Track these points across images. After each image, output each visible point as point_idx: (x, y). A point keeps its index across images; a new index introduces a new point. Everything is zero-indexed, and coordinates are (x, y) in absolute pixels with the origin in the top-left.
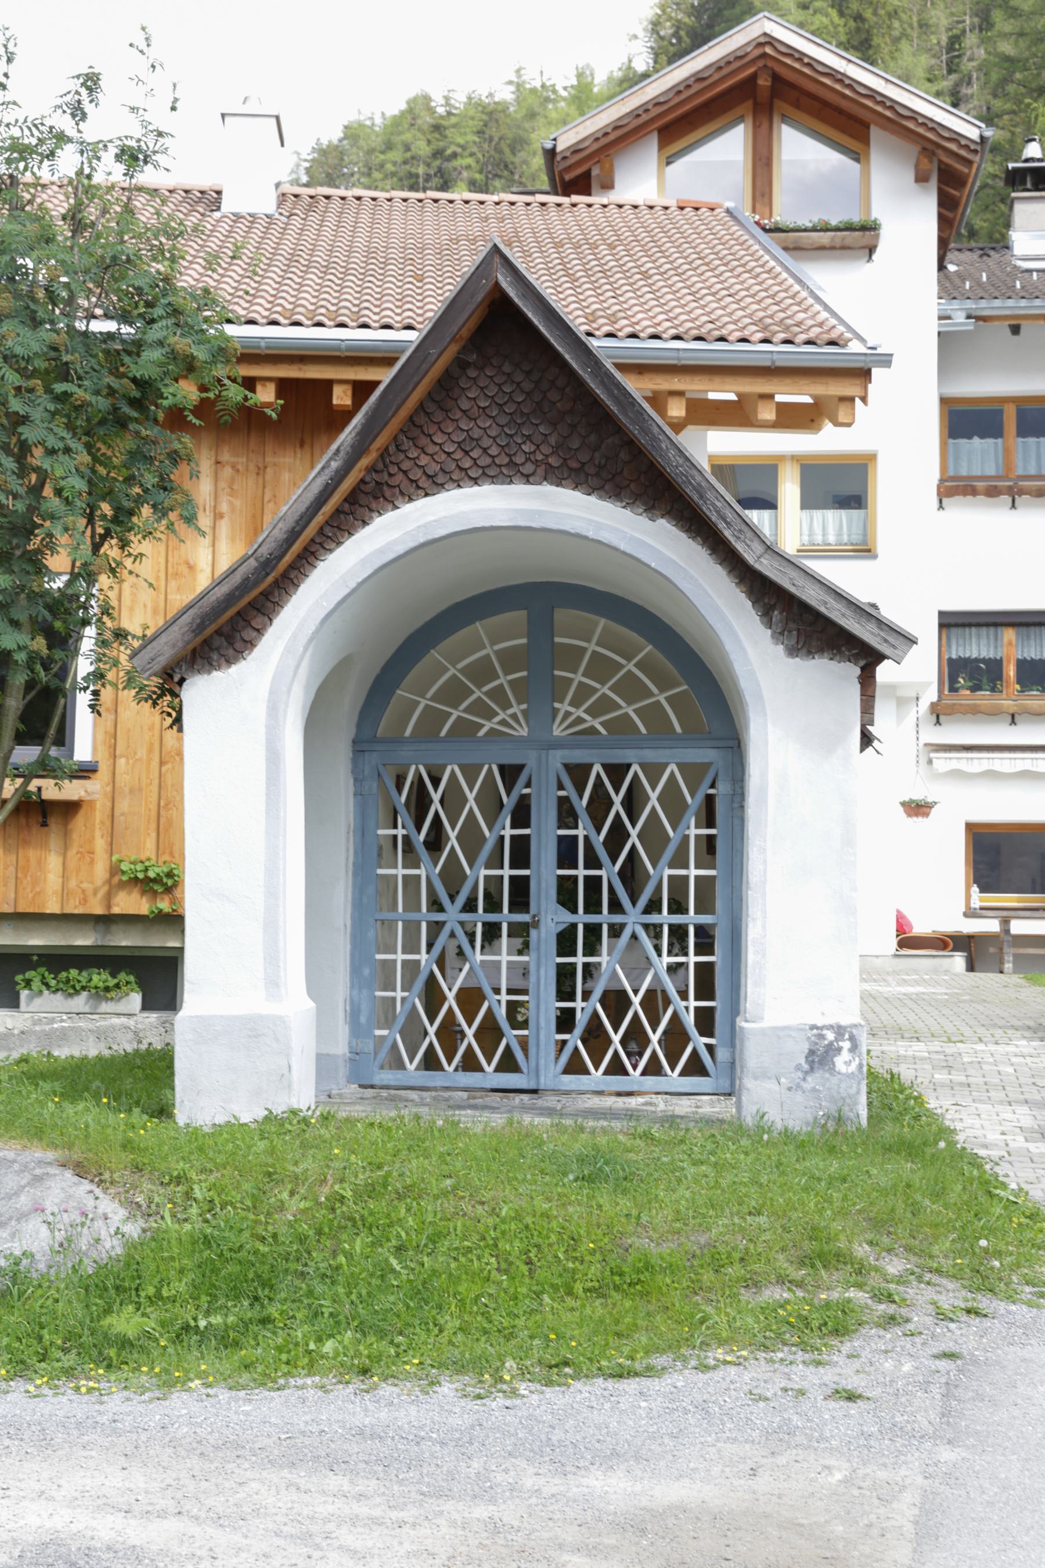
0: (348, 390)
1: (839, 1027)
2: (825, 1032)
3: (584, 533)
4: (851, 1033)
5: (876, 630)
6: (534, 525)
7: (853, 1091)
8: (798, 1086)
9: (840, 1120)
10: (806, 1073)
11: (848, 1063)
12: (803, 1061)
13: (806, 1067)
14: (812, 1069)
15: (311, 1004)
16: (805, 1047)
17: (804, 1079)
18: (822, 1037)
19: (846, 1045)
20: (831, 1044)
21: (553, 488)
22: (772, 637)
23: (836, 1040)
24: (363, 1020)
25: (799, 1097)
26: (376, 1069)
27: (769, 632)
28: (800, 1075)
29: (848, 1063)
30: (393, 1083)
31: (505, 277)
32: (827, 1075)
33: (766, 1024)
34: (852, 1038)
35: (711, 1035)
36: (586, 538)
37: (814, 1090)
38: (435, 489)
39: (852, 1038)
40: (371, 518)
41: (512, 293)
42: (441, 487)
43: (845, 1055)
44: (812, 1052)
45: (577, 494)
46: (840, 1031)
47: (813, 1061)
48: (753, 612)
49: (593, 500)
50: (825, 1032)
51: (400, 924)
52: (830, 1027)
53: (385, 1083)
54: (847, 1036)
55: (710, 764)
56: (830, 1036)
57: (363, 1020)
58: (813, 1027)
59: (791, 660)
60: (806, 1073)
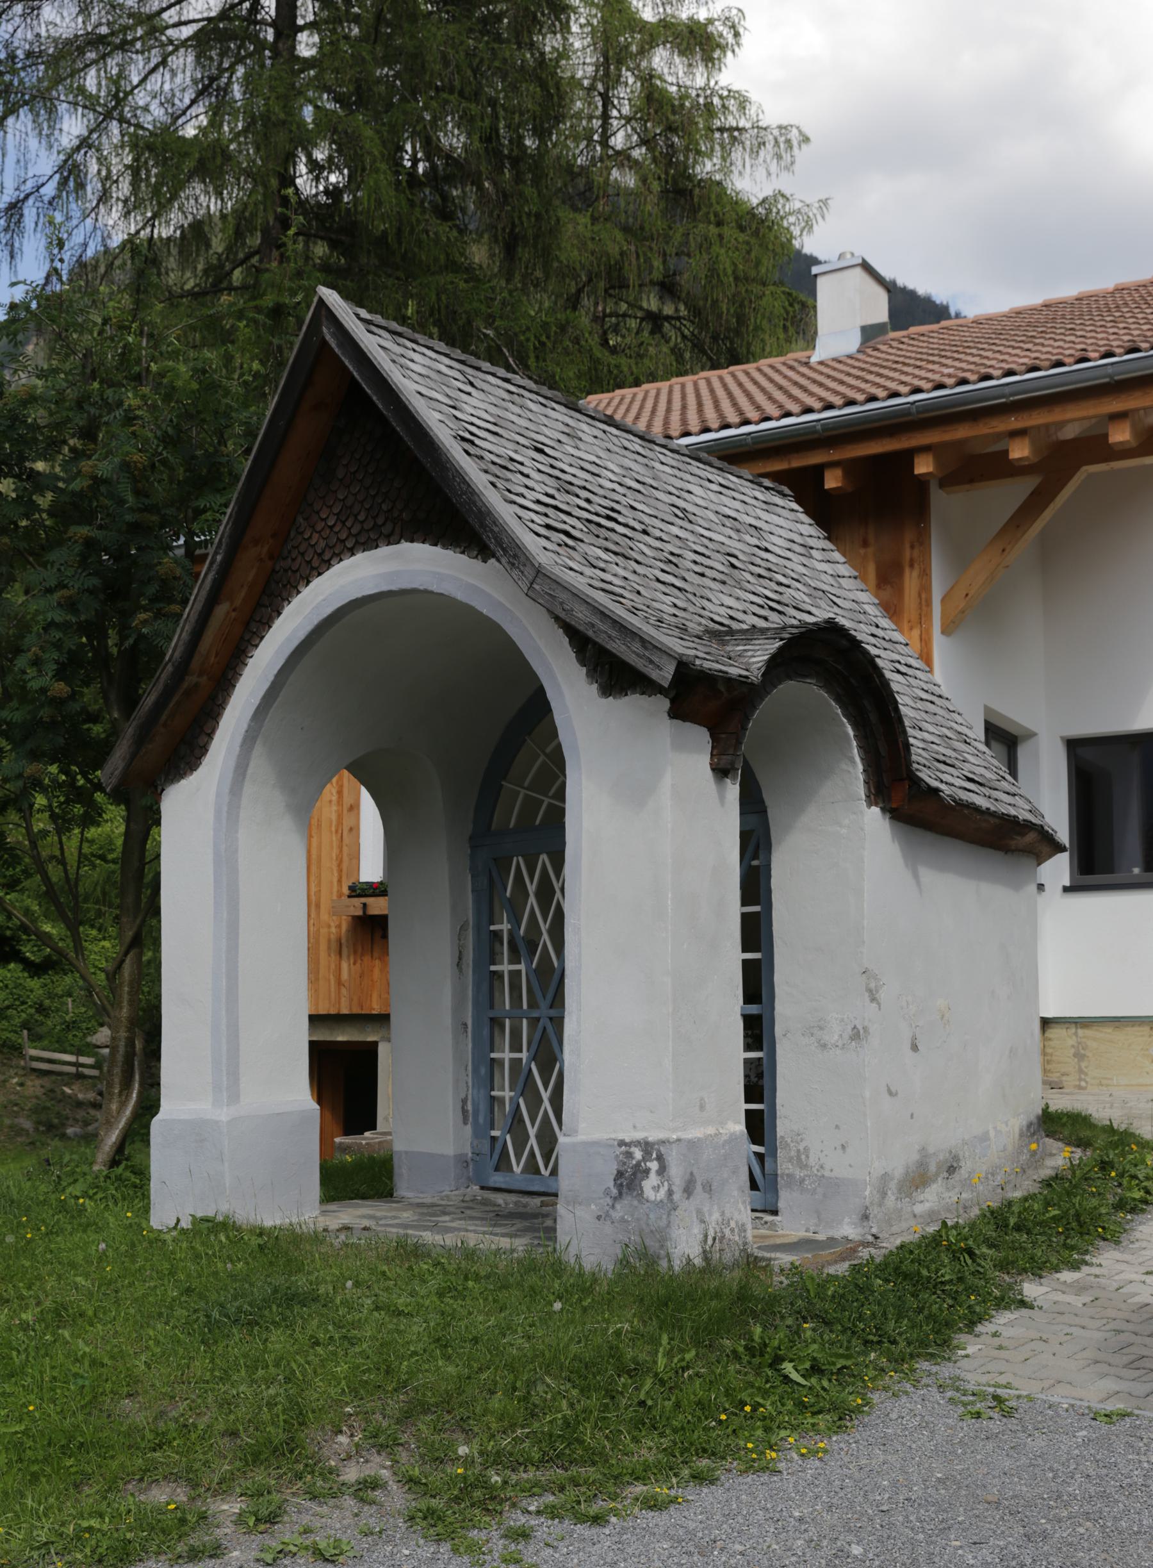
0: (838, 472)
1: (647, 1143)
2: (633, 1149)
3: (430, 588)
4: (659, 1151)
5: (641, 651)
6: (394, 588)
7: (663, 1223)
8: (607, 1215)
9: (650, 1260)
10: (615, 1199)
11: (656, 1189)
12: (611, 1184)
13: (615, 1191)
14: (620, 1194)
15: (318, 1107)
16: (613, 1168)
17: (613, 1207)
18: (629, 1155)
19: (654, 1166)
20: (638, 1164)
21: (408, 544)
22: (588, 674)
23: (644, 1159)
24: (481, 1120)
25: (608, 1228)
26: (491, 1171)
27: (584, 669)
28: (609, 1201)
29: (656, 1189)
30: (503, 1186)
31: (329, 329)
32: (635, 1203)
33: (581, 1137)
34: (660, 1158)
35: (761, 1144)
36: (432, 592)
37: (623, 1220)
38: (324, 566)
39: (660, 1158)
40: (283, 608)
41: (333, 343)
42: (328, 565)
43: (653, 1180)
44: (620, 1174)
45: (426, 547)
46: (647, 1147)
47: (621, 1185)
48: (570, 649)
49: (438, 550)
50: (633, 1149)
51: (525, 1022)
52: (637, 1143)
53: (497, 1185)
54: (654, 1156)
55: (753, 831)
56: (638, 1154)
57: (481, 1120)
58: (622, 1143)
59: (604, 701)
60: (615, 1199)
